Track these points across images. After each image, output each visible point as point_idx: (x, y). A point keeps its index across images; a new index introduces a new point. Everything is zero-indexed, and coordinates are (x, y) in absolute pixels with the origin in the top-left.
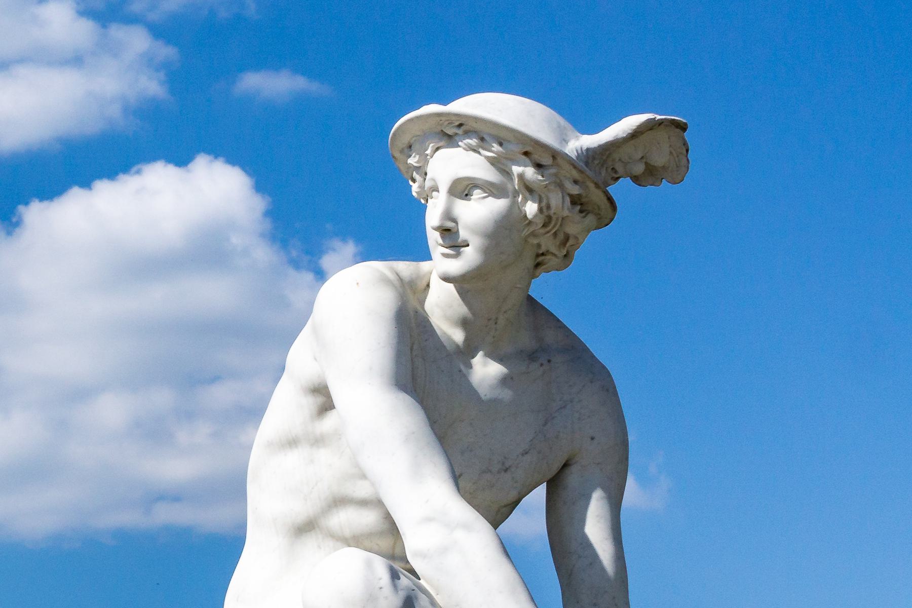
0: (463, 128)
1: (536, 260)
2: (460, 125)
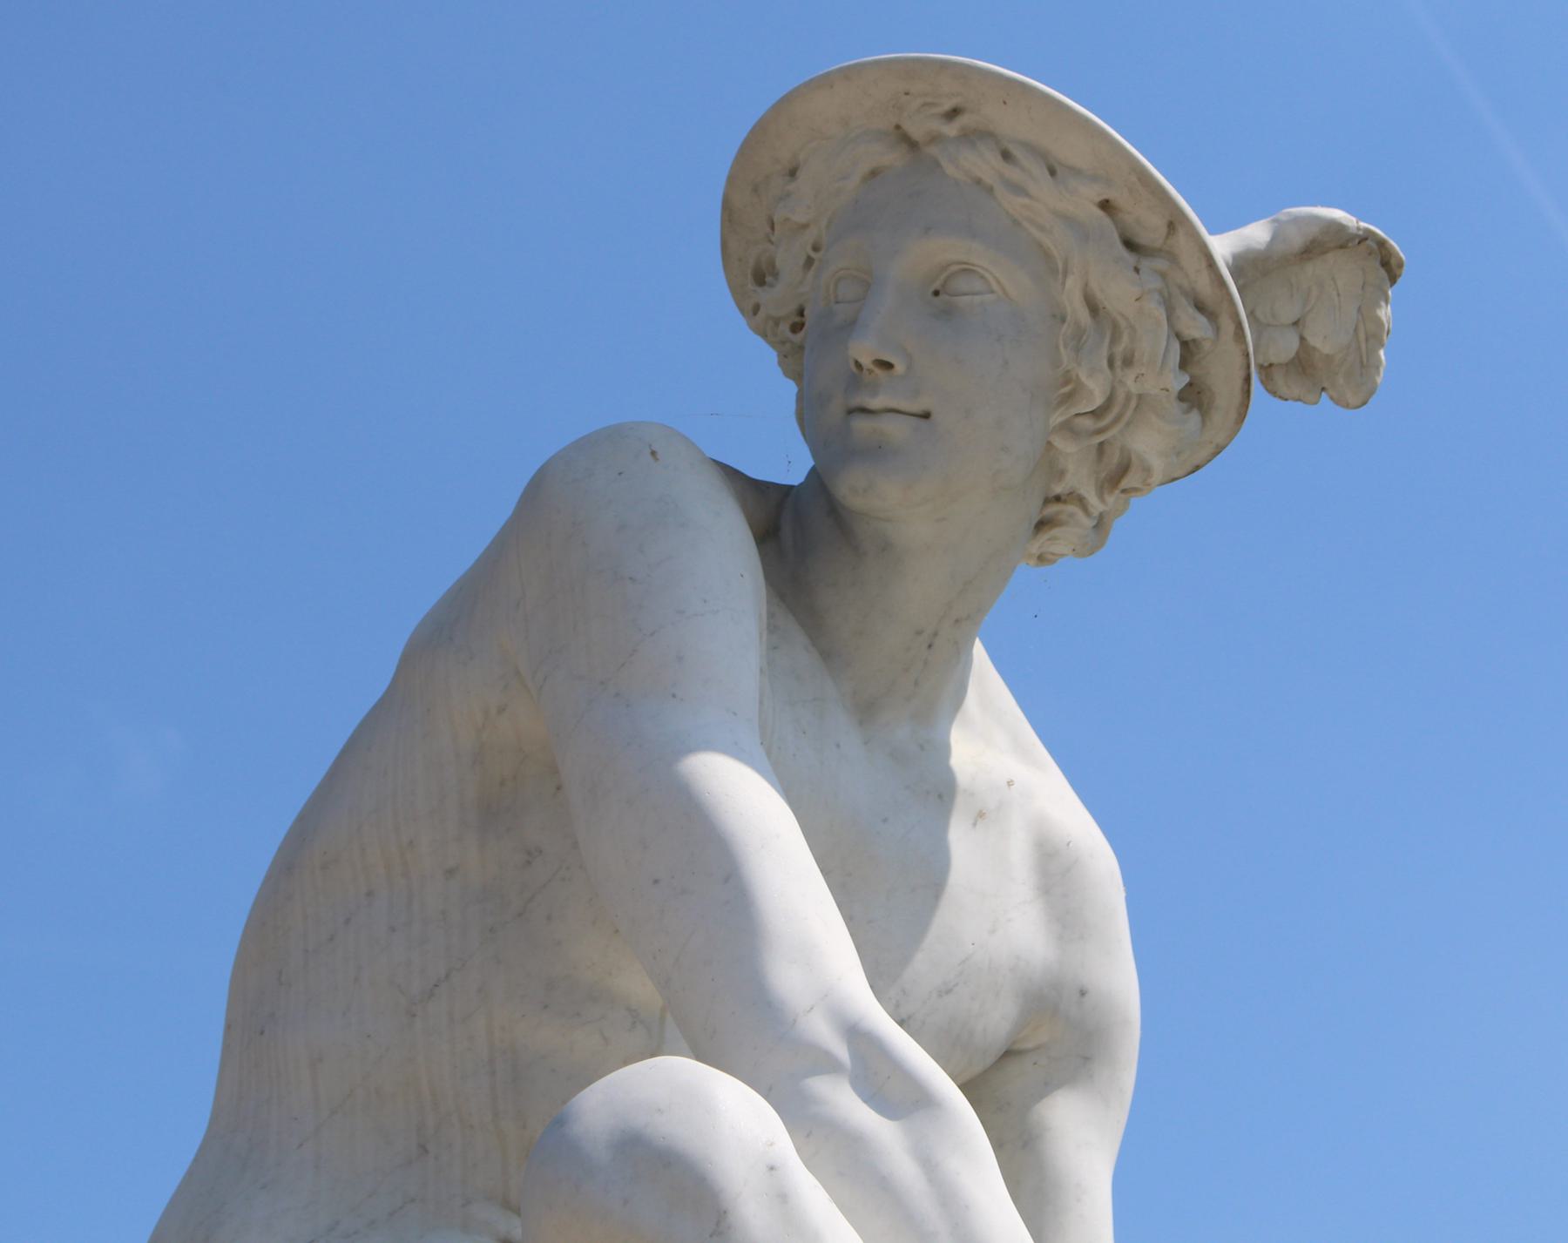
0: (963, 120)
2: (954, 113)
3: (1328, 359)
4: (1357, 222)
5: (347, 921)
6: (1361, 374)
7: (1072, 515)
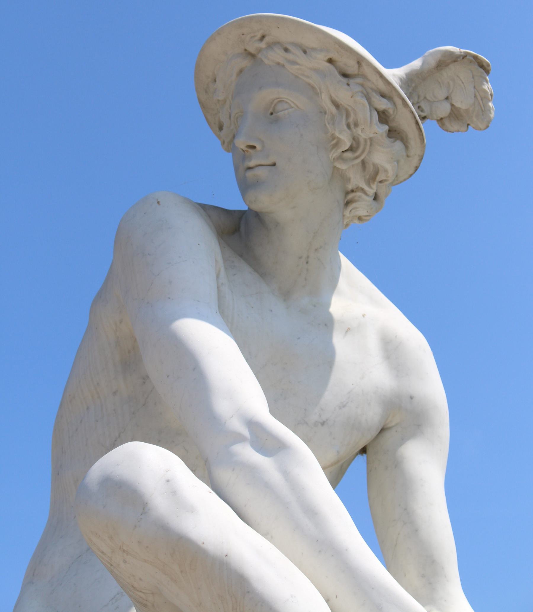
0: (267, 39)
1: (346, 197)
2: (263, 37)
3: (467, 111)
4: (460, 50)
5: (81, 422)
6: (483, 115)
7: (360, 197)
